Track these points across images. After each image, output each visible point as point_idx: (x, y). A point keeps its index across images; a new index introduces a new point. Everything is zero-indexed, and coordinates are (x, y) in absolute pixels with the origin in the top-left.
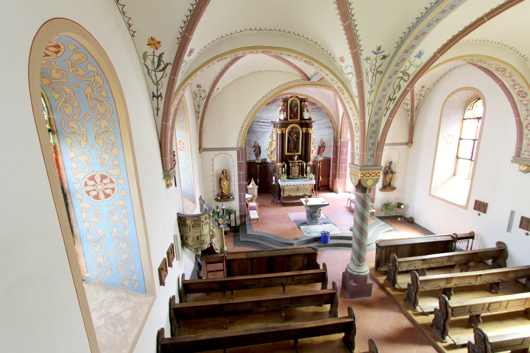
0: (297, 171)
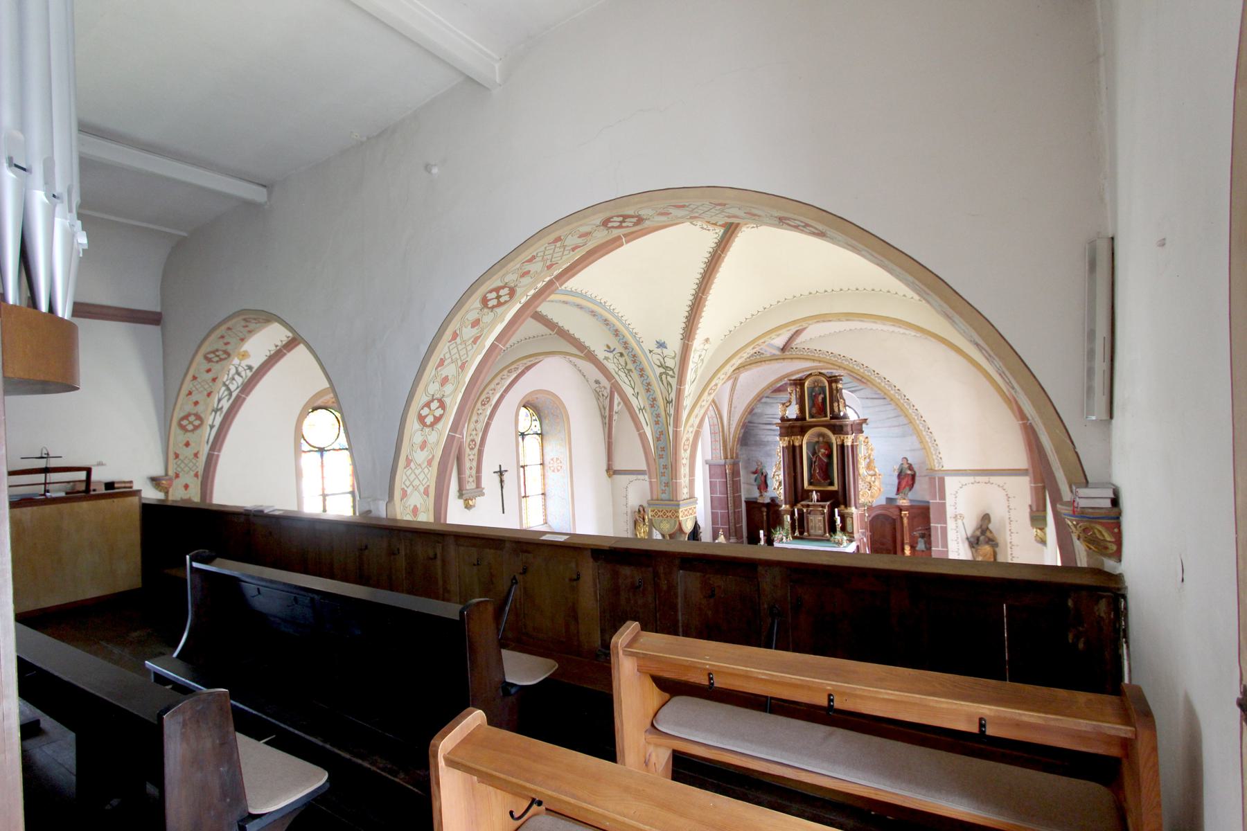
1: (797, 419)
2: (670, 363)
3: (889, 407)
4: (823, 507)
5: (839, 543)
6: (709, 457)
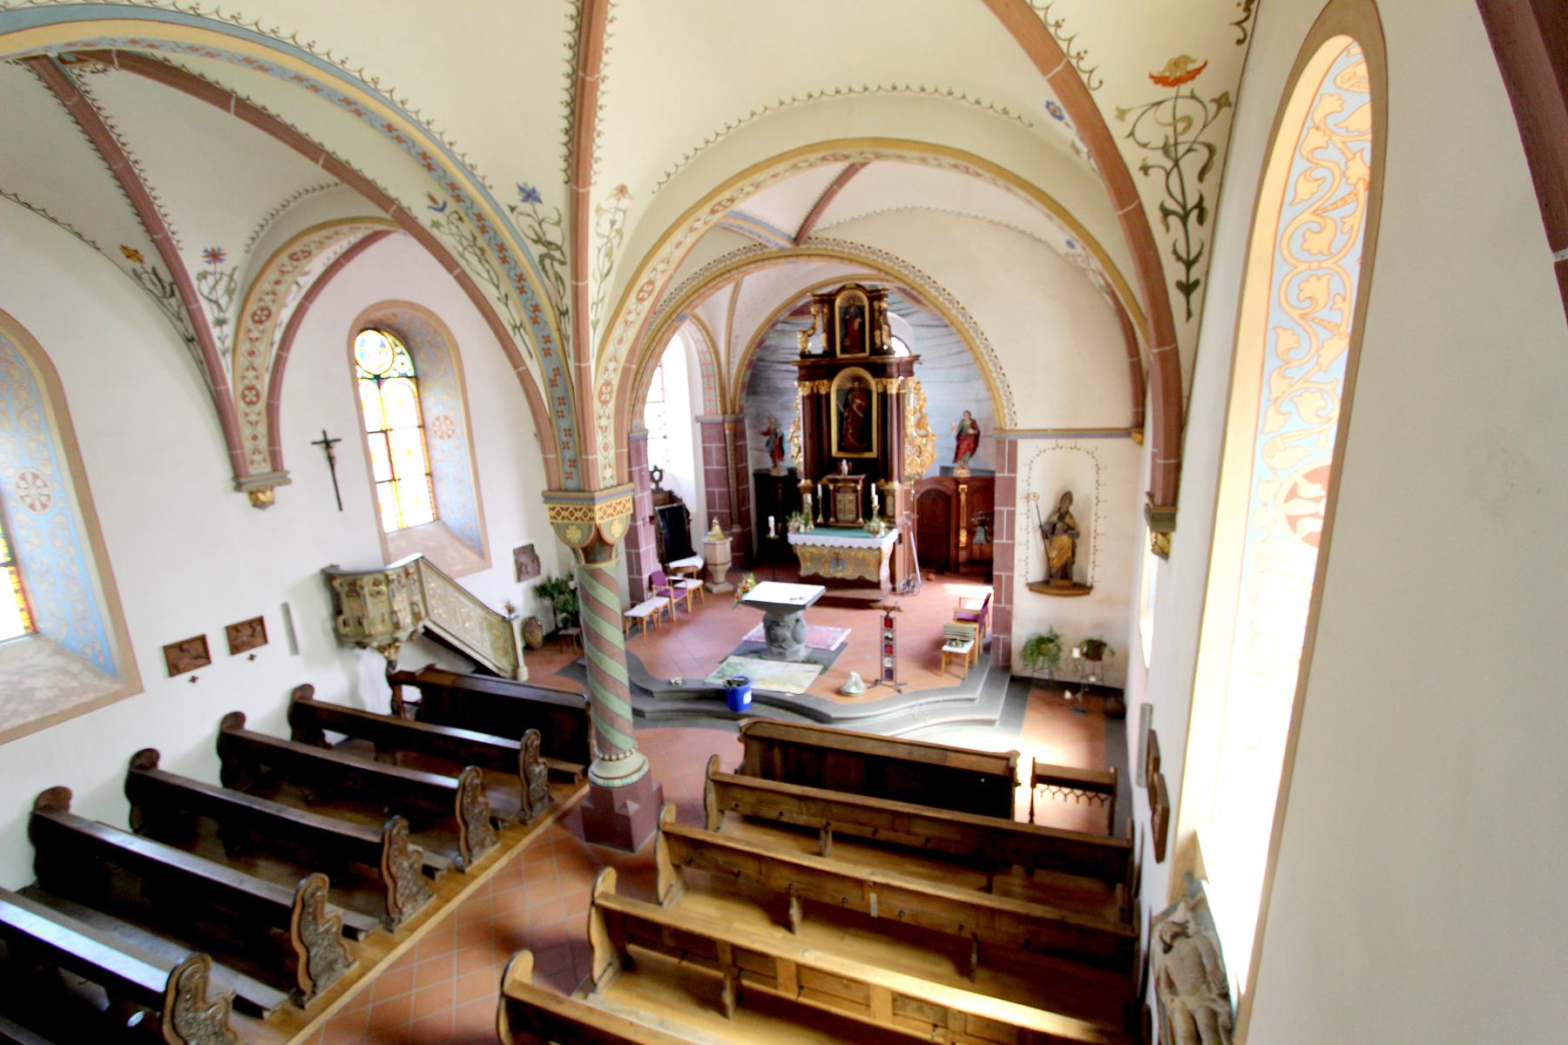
0: (853, 507)
1: (825, 354)
2: (555, 234)
3: (952, 339)
4: (856, 482)
5: (875, 533)
6: (700, 412)
